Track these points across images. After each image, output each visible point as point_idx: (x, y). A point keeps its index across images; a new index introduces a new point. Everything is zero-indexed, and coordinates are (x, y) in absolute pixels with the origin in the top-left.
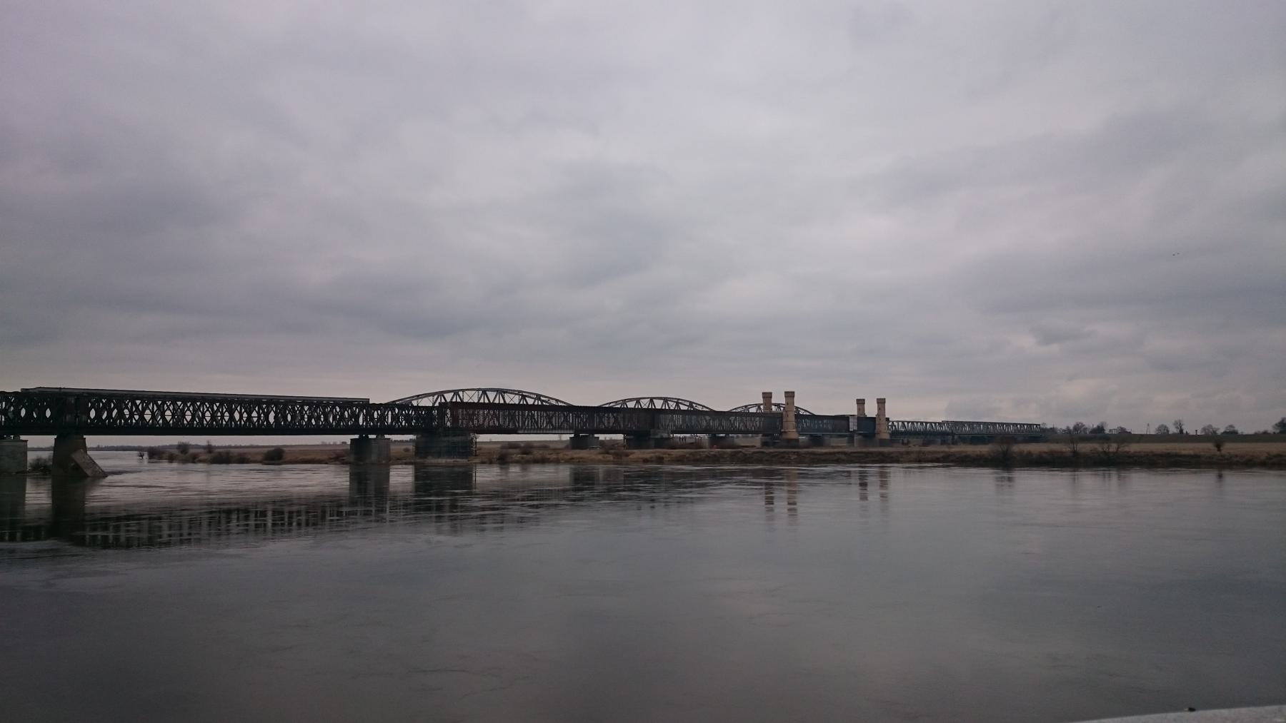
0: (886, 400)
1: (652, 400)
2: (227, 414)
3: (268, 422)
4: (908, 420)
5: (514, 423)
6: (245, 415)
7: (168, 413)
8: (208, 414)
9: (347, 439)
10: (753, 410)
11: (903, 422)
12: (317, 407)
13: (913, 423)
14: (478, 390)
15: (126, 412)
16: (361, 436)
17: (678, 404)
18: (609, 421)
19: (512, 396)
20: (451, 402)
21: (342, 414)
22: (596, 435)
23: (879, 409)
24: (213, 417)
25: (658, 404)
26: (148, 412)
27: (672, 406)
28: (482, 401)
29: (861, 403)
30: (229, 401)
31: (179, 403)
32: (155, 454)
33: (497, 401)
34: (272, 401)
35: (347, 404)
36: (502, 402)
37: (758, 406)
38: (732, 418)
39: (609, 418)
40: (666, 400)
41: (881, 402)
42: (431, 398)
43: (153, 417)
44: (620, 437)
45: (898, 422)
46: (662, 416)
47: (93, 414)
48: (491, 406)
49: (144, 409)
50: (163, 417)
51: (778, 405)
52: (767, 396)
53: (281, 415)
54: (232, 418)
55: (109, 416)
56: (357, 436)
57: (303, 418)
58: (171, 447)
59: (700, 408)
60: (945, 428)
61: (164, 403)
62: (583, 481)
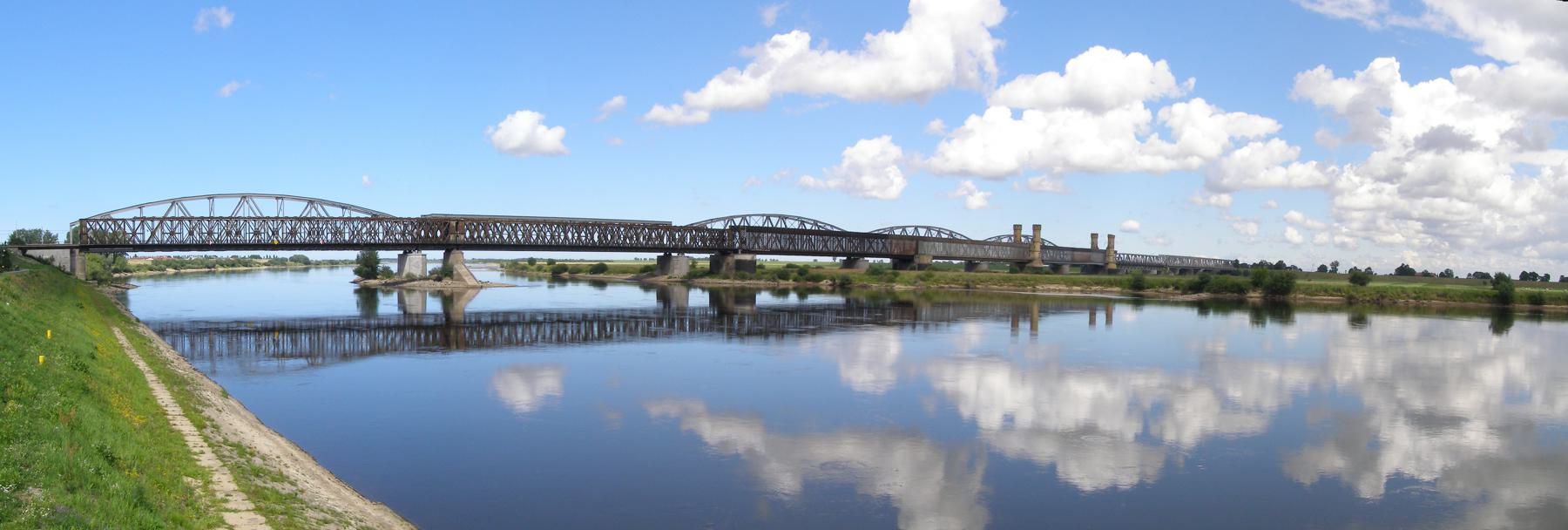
0: (1110, 233)
1: (916, 228)
2: (562, 234)
3: (593, 241)
4: (1147, 254)
5: (794, 245)
6: (576, 235)
7: (520, 233)
8: (548, 234)
9: (654, 255)
10: (1005, 240)
11: (1128, 255)
12: (631, 228)
13: (1135, 256)
14: (763, 215)
15: (490, 232)
16: (665, 253)
17: (939, 232)
18: (878, 246)
19: (792, 221)
20: (739, 225)
21: (651, 235)
22: (866, 259)
23: (1109, 243)
24: (552, 237)
25: (922, 232)
26: (505, 232)
27: (934, 234)
28: (766, 225)
29: (1094, 236)
30: (564, 224)
31: (527, 225)
32: (515, 270)
33: (779, 226)
34: (597, 224)
35: (655, 226)
36: (783, 226)
37: (1009, 236)
38: (987, 247)
39: (878, 243)
40: (929, 229)
41: (1111, 237)
42: (722, 222)
43: (509, 236)
44: (887, 261)
45: (1124, 254)
46: (926, 243)
47: (468, 234)
48: (773, 230)
49: (503, 230)
50: (516, 237)
51: (1026, 237)
52: (1017, 228)
53: (603, 235)
54: (566, 237)
55: (479, 236)
56: (662, 254)
57: (619, 237)
58: (523, 260)
59: (958, 237)
60: (1161, 261)
61: (516, 225)
62: (252, 454)
